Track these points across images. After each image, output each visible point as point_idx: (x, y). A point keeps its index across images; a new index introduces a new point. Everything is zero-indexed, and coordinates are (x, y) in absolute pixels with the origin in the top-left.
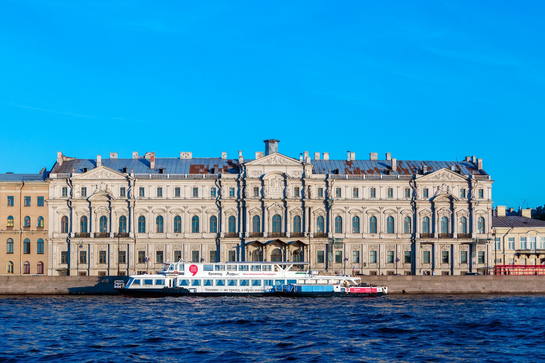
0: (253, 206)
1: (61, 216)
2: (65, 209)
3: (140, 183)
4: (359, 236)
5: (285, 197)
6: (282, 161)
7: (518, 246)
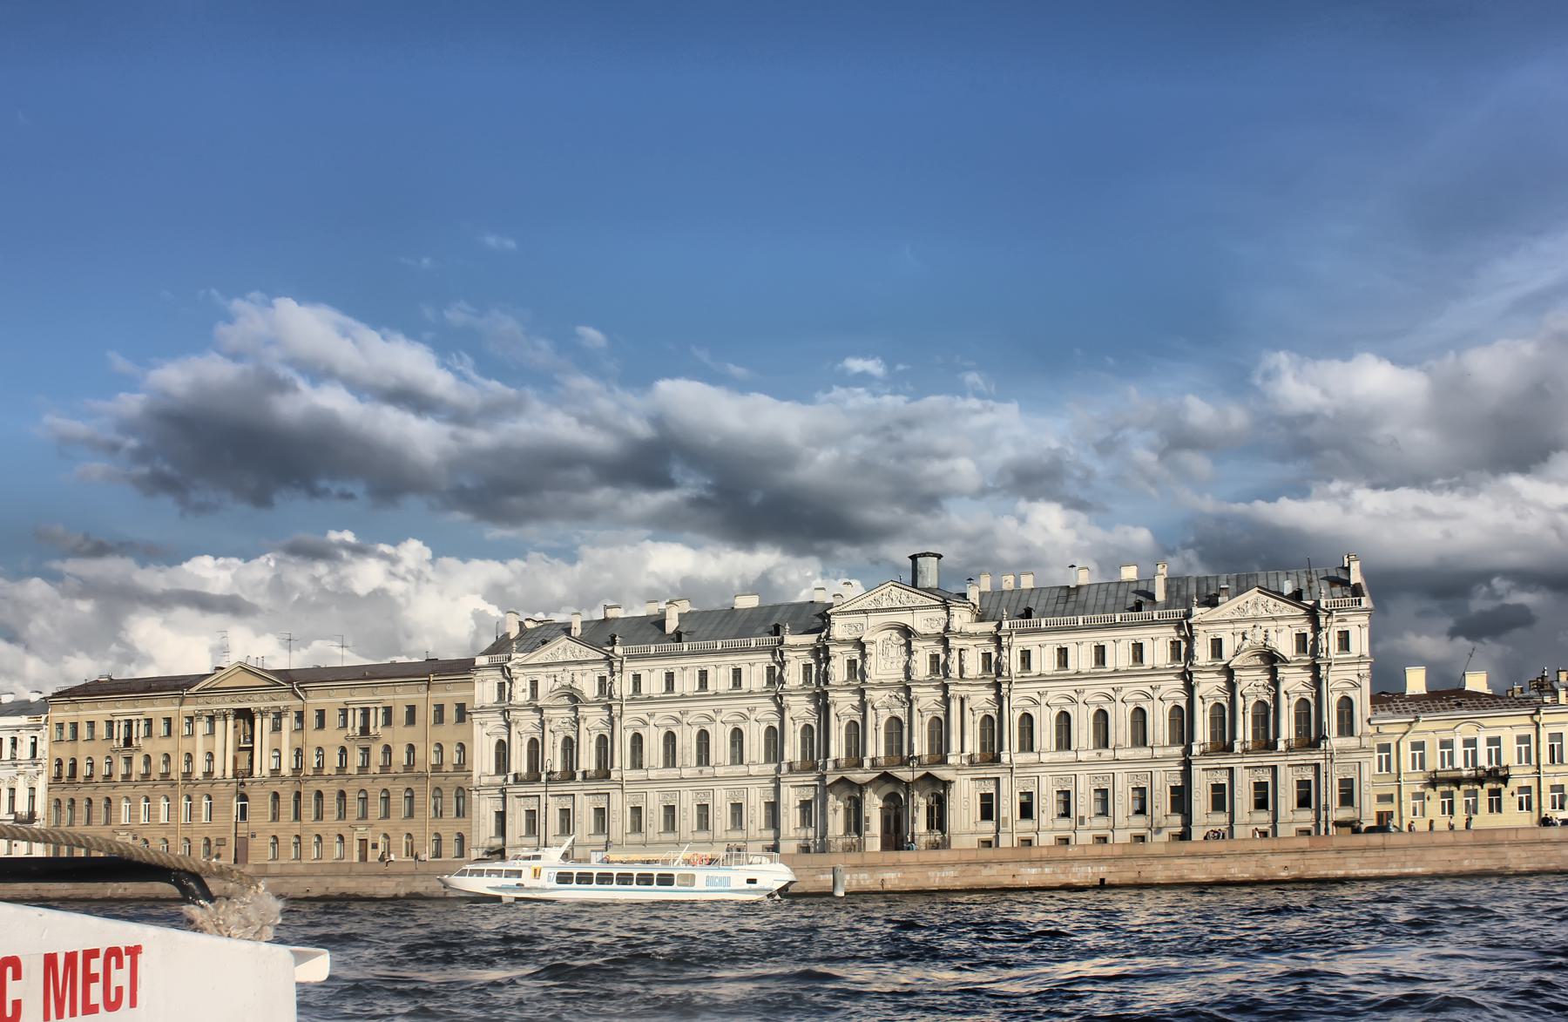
0: (843, 704)
1: (764, 726)
2: (988, 701)
3: (632, 667)
4: (1068, 756)
5: (908, 678)
6: (904, 598)
7: (1434, 762)
